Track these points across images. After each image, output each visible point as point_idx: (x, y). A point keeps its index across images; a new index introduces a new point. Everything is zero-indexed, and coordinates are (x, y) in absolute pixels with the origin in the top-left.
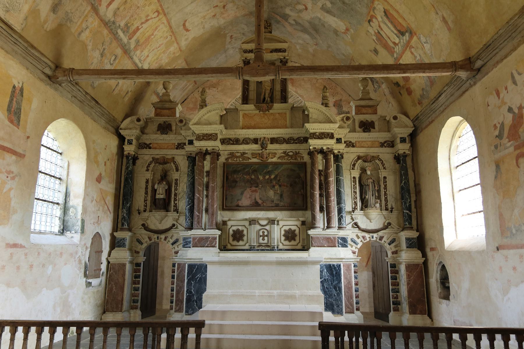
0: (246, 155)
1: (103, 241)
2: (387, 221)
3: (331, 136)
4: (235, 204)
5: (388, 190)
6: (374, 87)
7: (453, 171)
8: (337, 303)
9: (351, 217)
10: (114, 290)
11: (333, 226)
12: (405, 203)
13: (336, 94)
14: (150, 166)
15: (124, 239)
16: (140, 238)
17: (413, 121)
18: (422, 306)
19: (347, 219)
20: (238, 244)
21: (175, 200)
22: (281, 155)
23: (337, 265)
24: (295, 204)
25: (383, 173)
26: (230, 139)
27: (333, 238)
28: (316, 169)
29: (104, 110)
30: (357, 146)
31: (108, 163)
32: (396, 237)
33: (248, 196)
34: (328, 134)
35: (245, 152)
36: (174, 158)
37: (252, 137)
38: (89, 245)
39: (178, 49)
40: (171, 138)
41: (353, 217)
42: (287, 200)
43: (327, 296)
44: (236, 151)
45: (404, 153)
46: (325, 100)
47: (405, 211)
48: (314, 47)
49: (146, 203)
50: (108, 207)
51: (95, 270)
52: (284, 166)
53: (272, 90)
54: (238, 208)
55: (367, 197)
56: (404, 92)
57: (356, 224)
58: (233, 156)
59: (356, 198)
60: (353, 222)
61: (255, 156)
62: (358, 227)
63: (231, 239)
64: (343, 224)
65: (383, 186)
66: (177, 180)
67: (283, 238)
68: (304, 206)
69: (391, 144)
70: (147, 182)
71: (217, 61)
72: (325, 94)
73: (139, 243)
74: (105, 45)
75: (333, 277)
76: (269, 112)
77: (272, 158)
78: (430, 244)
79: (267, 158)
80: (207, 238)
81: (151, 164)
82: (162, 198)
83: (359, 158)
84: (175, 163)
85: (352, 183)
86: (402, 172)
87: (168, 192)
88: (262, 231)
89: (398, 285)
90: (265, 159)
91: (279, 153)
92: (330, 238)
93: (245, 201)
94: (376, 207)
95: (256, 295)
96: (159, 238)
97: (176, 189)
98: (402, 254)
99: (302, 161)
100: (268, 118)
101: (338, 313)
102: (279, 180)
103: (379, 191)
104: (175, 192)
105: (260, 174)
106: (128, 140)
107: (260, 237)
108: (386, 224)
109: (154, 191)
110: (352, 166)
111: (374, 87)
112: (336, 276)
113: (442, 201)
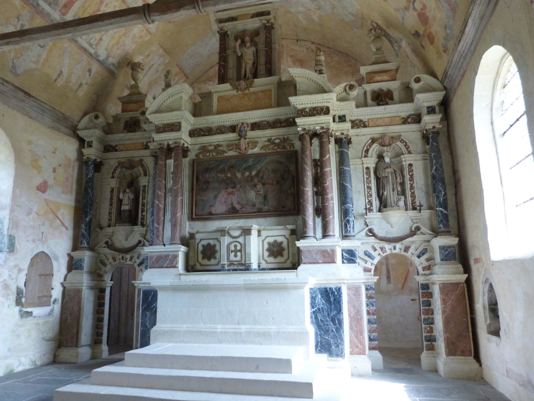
0: (221, 148)
1: (55, 264)
2: (415, 225)
3: (326, 111)
4: (206, 211)
5: (415, 181)
6: (395, 50)
7: (499, 140)
8: (336, 341)
9: (364, 222)
10: (69, 321)
11: (331, 233)
12: (438, 197)
13: (357, 73)
14: (115, 172)
15: (81, 260)
16: (104, 258)
17: (442, 82)
18: (464, 345)
19: (357, 226)
20: (209, 263)
21: (143, 211)
22: (264, 144)
23: (335, 289)
24: (283, 207)
25: (407, 159)
26: (201, 129)
27: (330, 250)
28: (306, 157)
29: (42, 104)
30: (370, 125)
31: (60, 170)
32: (428, 246)
33: (223, 200)
34: (322, 109)
35: (219, 144)
36: (141, 160)
37: (228, 124)
38: (25, 265)
39: (145, 31)
40: (136, 137)
41: (367, 222)
42: (272, 202)
43: (322, 332)
44: (208, 144)
45: (434, 127)
46: (318, 65)
47: (438, 209)
48: (318, 12)
49: (111, 217)
50: (61, 222)
51: (39, 297)
52: (268, 158)
53: (256, 64)
54: (210, 216)
55: (385, 193)
56: (426, 42)
57: (371, 231)
58: (205, 150)
59: (371, 195)
60: (367, 228)
61: (231, 148)
62: (374, 235)
63: (200, 256)
64: (350, 231)
65: (408, 177)
66: (146, 187)
67: (266, 254)
68: (294, 210)
69: (417, 118)
70: (112, 191)
71: (208, 48)
72: (319, 58)
73: (103, 264)
74: (22, 20)
75: (330, 304)
76: (249, 90)
77: (253, 149)
78: (474, 254)
79: (246, 149)
80: (167, 256)
81: (117, 170)
82: (127, 209)
83: (373, 141)
84: (143, 166)
85: (365, 176)
86: (432, 154)
87: (136, 202)
88: (234, 244)
89: (433, 314)
90: (243, 151)
91: (262, 142)
92: (326, 251)
93: (220, 207)
94: (399, 206)
95: (217, 332)
96: (124, 258)
97: (144, 198)
98: (435, 270)
99: (292, 149)
100: (249, 99)
101: (337, 356)
102: (262, 178)
103: (403, 184)
104: (143, 201)
105: (239, 171)
106: (88, 142)
107: (231, 252)
108: (413, 229)
109: (120, 202)
110: (364, 153)
111: (395, 50)
112: (334, 304)
113: (483, 188)
